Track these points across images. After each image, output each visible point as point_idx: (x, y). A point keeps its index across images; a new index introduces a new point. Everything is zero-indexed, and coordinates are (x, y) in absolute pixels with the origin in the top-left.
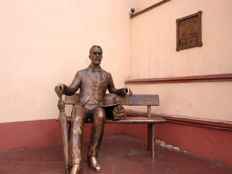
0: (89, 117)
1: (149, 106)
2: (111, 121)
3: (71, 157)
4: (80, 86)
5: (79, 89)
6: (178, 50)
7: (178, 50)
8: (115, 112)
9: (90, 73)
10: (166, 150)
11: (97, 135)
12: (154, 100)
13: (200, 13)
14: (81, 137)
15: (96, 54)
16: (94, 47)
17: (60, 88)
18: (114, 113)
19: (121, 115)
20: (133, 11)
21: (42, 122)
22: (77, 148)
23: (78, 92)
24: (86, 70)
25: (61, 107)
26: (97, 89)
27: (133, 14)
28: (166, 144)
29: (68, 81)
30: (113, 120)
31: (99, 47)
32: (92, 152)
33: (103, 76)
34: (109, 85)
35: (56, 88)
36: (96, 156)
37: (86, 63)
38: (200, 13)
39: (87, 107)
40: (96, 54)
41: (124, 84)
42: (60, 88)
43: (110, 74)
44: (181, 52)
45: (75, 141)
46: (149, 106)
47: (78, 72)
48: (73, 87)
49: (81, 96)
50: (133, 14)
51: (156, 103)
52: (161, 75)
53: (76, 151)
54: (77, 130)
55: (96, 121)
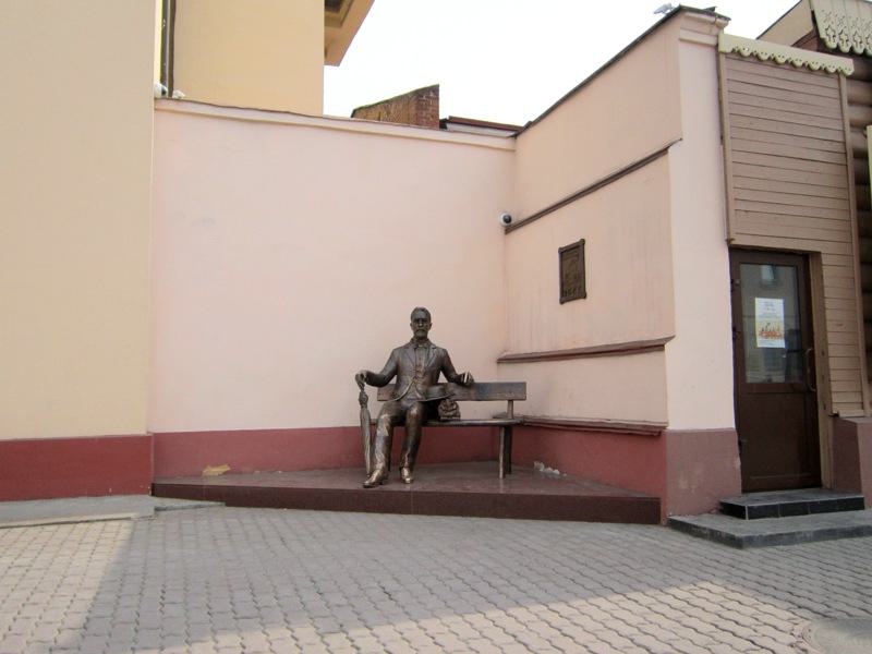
0: (399, 420)
1: (511, 401)
2: (437, 423)
3: (373, 463)
4: (397, 371)
5: (395, 378)
6: (562, 303)
7: (562, 303)
8: (441, 409)
9: (410, 351)
10: (546, 475)
11: (411, 440)
12: (515, 391)
13: (583, 242)
14: (389, 441)
15: (421, 321)
16: (416, 310)
17: (362, 375)
18: (440, 411)
19: (451, 413)
20: (508, 220)
21: (344, 429)
22: (380, 451)
23: (394, 381)
24: (406, 347)
25: (363, 401)
26: (420, 376)
27: (510, 225)
28: (546, 467)
29: (377, 368)
30: (439, 421)
31: (423, 310)
32: (404, 462)
33: (431, 355)
34: (444, 364)
35: (357, 376)
36: (411, 469)
37: (408, 335)
38: (583, 241)
39: (404, 403)
40: (421, 321)
41: (495, 365)
42: (362, 375)
43: (445, 351)
44: (567, 305)
45: (380, 445)
46: (511, 401)
47: (393, 353)
48: (386, 374)
49: (397, 386)
50: (510, 225)
51: (520, 396)
52: (598, 341)
53: (380, 457)
54: (383, 431)
55: (408, 421)
